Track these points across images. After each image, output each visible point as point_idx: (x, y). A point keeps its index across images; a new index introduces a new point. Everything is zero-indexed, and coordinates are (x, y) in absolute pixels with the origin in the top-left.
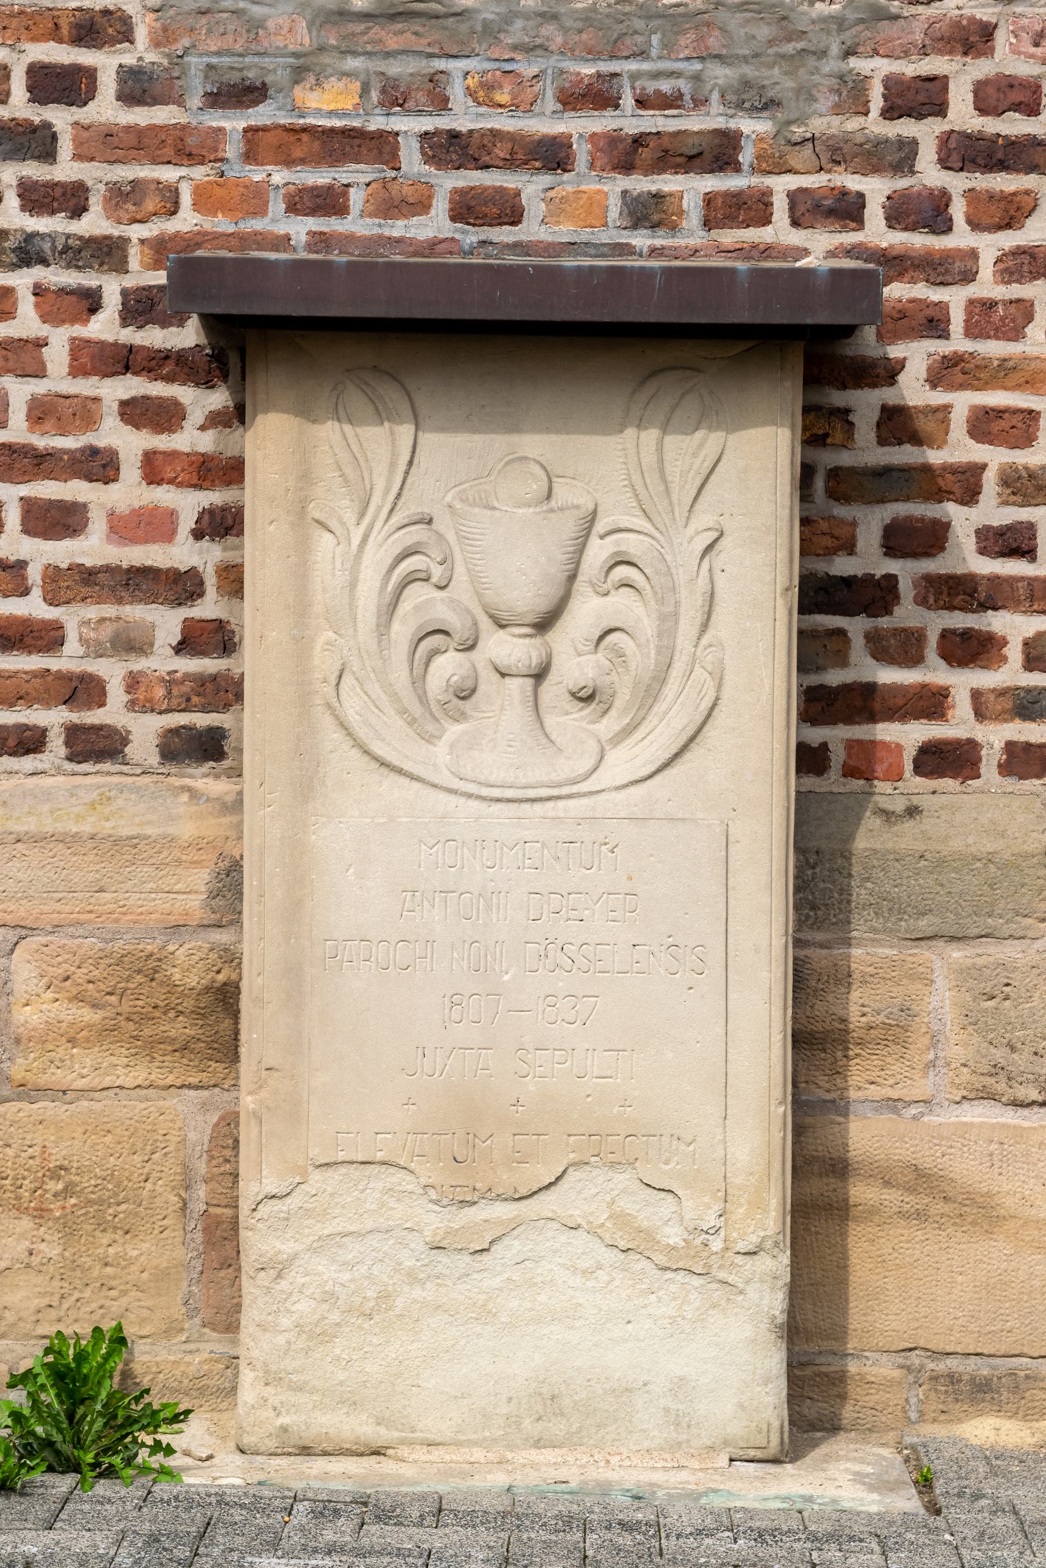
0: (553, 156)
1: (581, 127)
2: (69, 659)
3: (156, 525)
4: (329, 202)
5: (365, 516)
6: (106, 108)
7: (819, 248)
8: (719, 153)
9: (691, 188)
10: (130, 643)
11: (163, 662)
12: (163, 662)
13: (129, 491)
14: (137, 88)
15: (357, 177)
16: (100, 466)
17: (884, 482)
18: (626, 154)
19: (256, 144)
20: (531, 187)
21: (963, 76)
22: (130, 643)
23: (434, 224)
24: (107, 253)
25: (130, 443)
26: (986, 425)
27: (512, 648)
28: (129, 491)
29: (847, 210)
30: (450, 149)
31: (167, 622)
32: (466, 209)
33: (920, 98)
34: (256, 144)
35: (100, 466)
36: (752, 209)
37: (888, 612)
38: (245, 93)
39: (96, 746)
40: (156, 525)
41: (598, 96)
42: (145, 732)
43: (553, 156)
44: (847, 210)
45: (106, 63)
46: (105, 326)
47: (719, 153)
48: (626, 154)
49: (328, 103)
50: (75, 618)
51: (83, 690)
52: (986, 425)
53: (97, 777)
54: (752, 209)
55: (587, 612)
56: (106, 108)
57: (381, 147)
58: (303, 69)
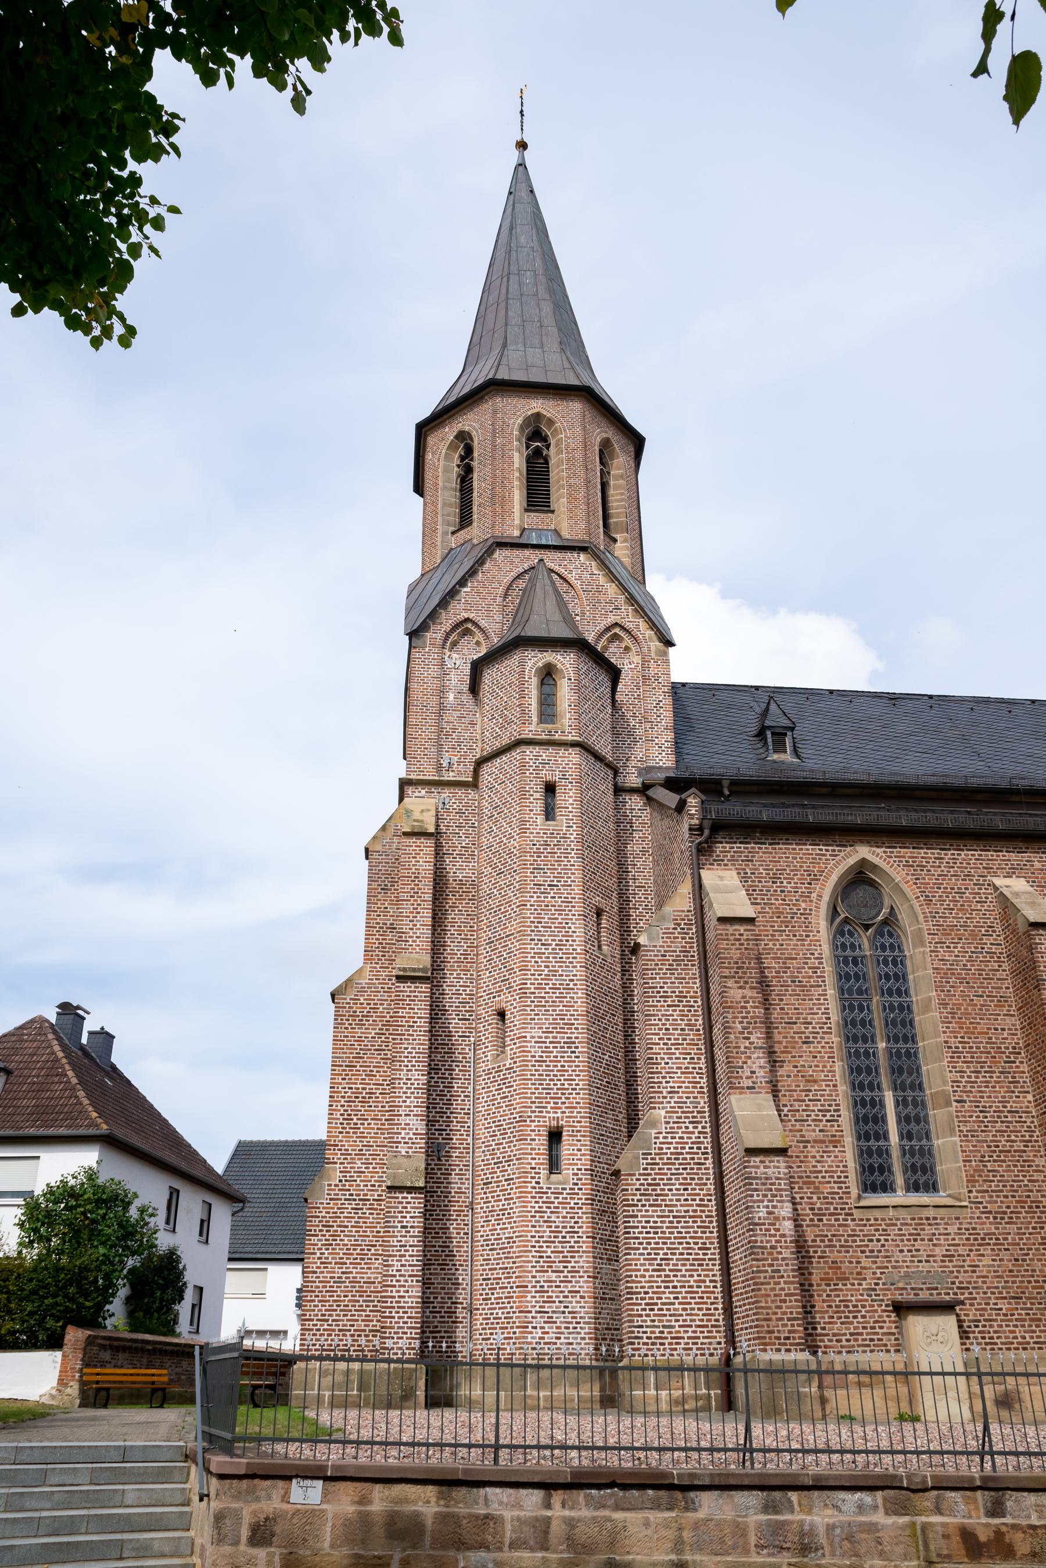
0: (922, 1289)
1: (924, 1286)
2: (884, 1342)
3: (890, 1328)
4: (902, 1294)
5: (918, 1325)
6: (881, 1286)
7: (947, 1298)
8: (936, 1289)
9: (935, 1292)
10: (890, 1340)
11: (893, 1342)
12: (893, 1342)
13: (887, 1324)
14: (884, 1284)
15: (904, 1292)
16: (885, 1322)
17: (810, 1312)
18: (928, 1289)
19: (895, 1289)
20: (920, 1292)
21: (957, 1281)
22: (890, 1340)
23: (912, 1296)
24: (882, 1300)
25: (887, 1319)
26: (965, 1315)
27: (934, 1338)
28: (887, 1324)
29: (949, 1294)
30: (912, 1289)
31: (893, 1338)
32: (915, 1295)
33: (953, 1283)
34: (895, 1289)
35: (885, 1322)
36: (940, 1294)
37: (90, 1336)
38: (893, 1284)
39: (888, 1351)
40: (890, 1328)
41: (925, 1283)
42: (892, 1349)
43: (922, 1289)
44: (949, 1294)
45: (880, 1282)
46: (883, 1307)
47: (936, 1289)
48: (928, 1289)
49: (901, 1285)
50: (884, 1338)
51: (886, 1345)
52: (965, 1315)
53: (888, 1355)
54: (940, 1294)
55: (940, 1334)
56: (881, 1286)
57: (906, 1289)
58: (898, 1281)
